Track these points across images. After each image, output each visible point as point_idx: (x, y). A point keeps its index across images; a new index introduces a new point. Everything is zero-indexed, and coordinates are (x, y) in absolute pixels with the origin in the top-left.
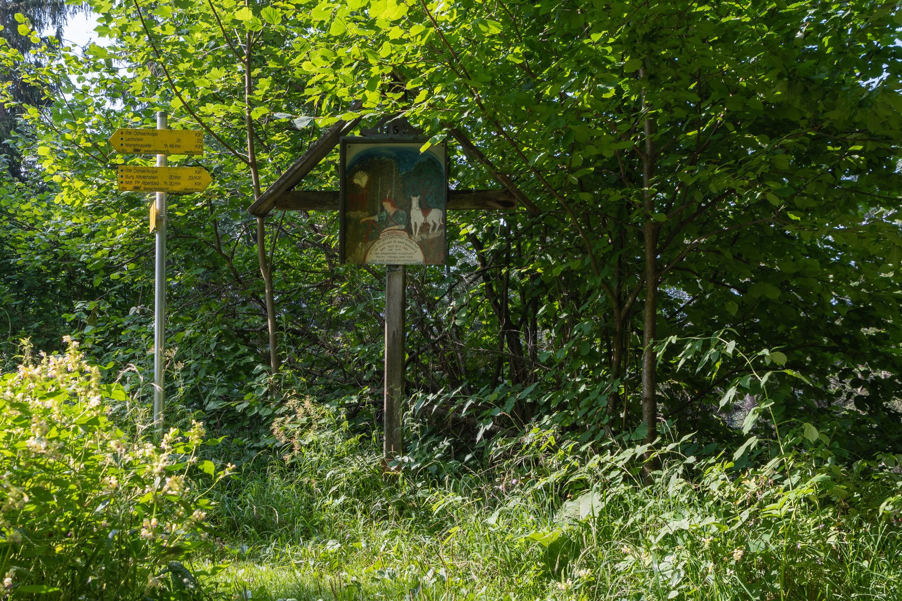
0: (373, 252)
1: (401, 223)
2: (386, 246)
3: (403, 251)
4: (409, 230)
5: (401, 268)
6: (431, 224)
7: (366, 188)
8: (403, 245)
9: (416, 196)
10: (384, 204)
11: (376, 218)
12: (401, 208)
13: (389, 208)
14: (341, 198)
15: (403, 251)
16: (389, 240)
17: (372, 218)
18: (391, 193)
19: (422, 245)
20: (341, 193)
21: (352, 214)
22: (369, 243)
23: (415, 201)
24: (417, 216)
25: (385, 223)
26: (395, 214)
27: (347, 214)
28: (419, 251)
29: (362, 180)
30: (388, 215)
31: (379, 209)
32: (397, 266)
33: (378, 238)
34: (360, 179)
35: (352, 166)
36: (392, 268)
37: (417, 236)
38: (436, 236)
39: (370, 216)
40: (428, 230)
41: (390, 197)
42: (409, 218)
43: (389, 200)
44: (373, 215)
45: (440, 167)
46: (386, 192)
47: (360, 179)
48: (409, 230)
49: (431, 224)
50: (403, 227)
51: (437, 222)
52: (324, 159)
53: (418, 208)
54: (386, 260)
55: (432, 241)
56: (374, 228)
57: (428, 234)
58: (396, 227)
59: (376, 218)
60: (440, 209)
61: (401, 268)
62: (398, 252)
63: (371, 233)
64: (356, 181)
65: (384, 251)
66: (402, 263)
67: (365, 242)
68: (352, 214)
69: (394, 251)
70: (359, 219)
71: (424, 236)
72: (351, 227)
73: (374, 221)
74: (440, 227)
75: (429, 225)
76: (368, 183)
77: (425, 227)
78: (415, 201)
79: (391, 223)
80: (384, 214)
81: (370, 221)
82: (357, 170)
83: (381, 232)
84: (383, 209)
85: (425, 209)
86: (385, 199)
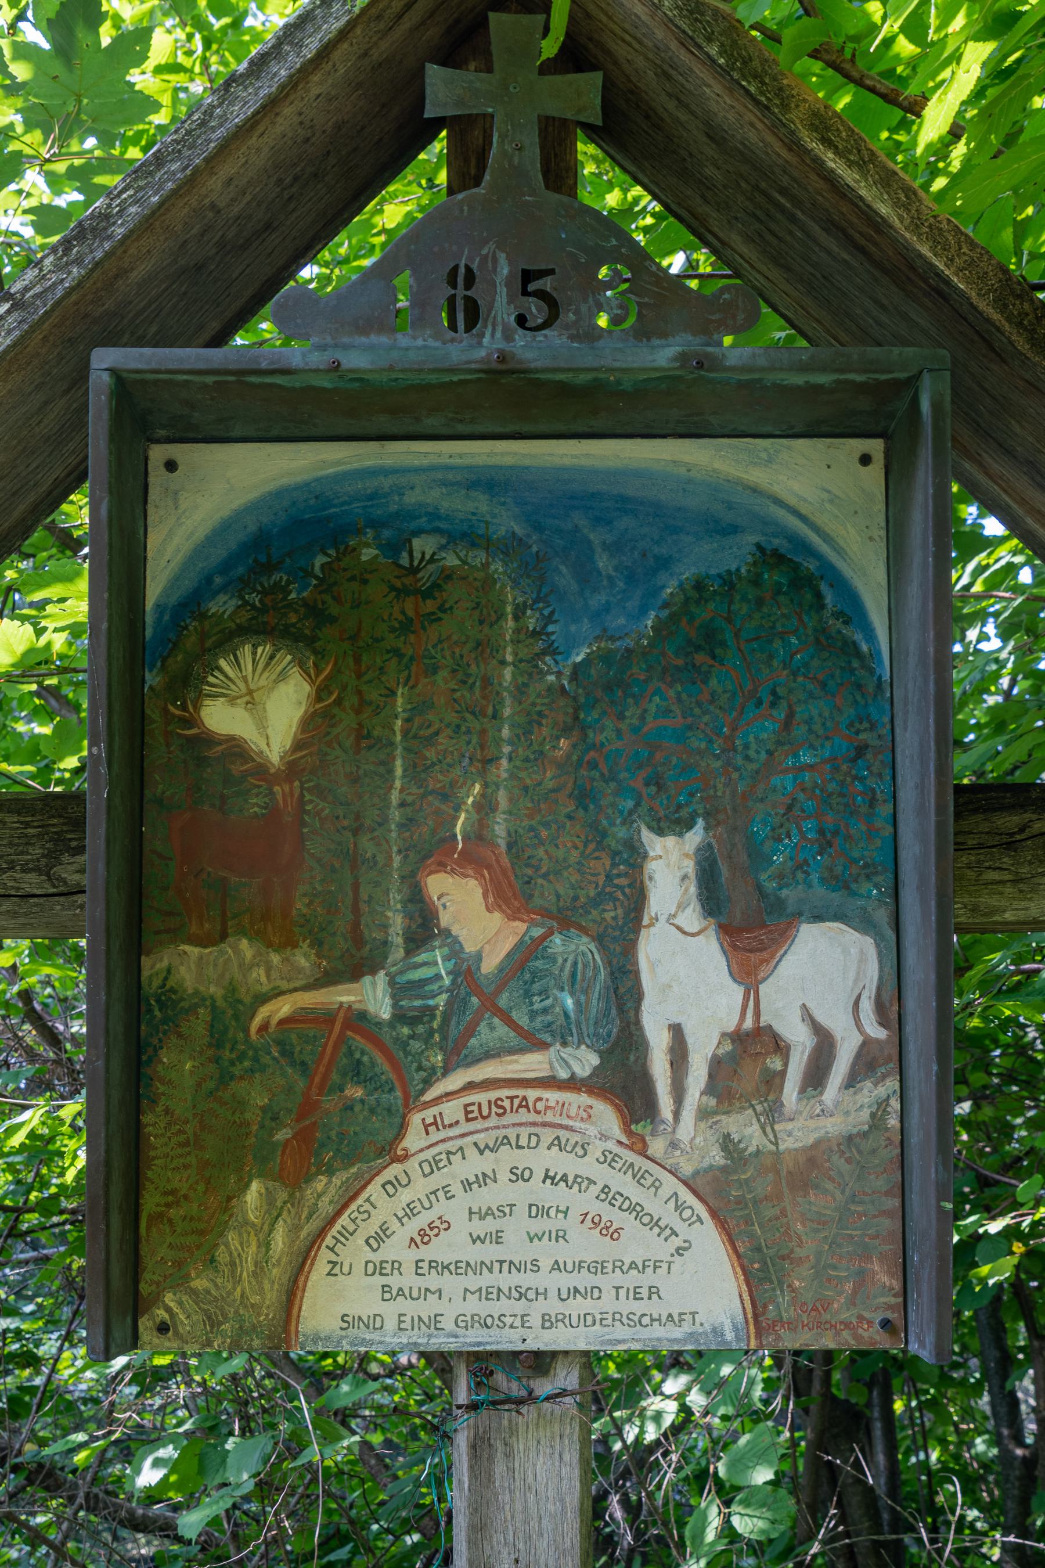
0: (356, 1253)
1: (564, 1033)
2: (454, 1210)
3: (586, 1245)
4: (626, 1086)
5: (567, 1377)
6: (799, 1038)
7: (292, 769)
8: (586, 1201)
9: (674, 823)
10: (438, 885)
11: (373, 995)
12: (564, 919)
13: (474, 920)
14: (96, 831)
15: (586, 1245)
16: (474, 1164)
17: (344, 996)
18: (485, 807)
19: (732, 1197)
20: (268, 308)
21: (185, 966)
22: (323, 1189)
23: (670, 866)
24: (686, 981)
25: (444, 1029)
26: (525, 959)
27: (152, 966)
28: (708, 1242)
29: (262, 709)
30: (466, 972)
31: (397, 923)
32: (540, 1362)
33: (389, 1151)
34: (251, 701)
35: (189, 606)
36: (500, 1378)
37: (689, 1131)
38: (834, 1126)
39: (328, 979)
40: (774, 1081)
41: (479, 835)
42: (624, 991)
43: (472, 859)
44: (356, 970)
45: (853, 611)
46: (449, 796)
47: (251, 701)
48: (626, 1086)
49: (799, 1038)
50: (585, 1061)
51: (838, 1022)
52: (1023, 1330)
53: (692, 918)
54: (459, 1316)
55: (809, 1169)
56: (357, 1072)
57: (773, 1113)
58: (532, 1064)
59: (373, 995)
60: (865, 924)
61: (567, 1377)
62: (546, 1253)
63: (337, 1114)
64: (220, 717)
65: (439, 1250)
66: (578, 1339)
67: (294, 1169)
68: (185, 966)
69: (515, 1247)
70: (240, 1006)
71: (746, 1128)
72: (179, 1066)
73: (358, 1020)
74: (866, 1063)
75: (780, 1047)
76: (316, 726)
77: (751, 1052)
78: (670, 866)
79: (492, 1032)
80: (436, 962)
81: (324, 1018)
82: (228, 639)
83: (411, 1102)
84: (424, 927)
85: (748, 924)
86: (435, 852)
